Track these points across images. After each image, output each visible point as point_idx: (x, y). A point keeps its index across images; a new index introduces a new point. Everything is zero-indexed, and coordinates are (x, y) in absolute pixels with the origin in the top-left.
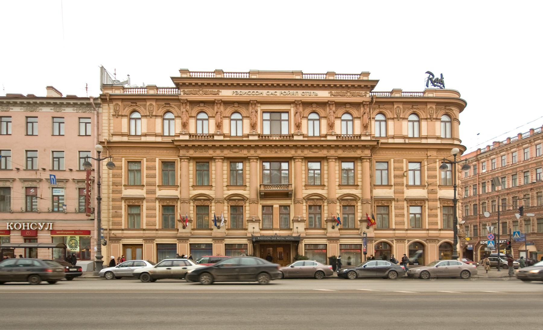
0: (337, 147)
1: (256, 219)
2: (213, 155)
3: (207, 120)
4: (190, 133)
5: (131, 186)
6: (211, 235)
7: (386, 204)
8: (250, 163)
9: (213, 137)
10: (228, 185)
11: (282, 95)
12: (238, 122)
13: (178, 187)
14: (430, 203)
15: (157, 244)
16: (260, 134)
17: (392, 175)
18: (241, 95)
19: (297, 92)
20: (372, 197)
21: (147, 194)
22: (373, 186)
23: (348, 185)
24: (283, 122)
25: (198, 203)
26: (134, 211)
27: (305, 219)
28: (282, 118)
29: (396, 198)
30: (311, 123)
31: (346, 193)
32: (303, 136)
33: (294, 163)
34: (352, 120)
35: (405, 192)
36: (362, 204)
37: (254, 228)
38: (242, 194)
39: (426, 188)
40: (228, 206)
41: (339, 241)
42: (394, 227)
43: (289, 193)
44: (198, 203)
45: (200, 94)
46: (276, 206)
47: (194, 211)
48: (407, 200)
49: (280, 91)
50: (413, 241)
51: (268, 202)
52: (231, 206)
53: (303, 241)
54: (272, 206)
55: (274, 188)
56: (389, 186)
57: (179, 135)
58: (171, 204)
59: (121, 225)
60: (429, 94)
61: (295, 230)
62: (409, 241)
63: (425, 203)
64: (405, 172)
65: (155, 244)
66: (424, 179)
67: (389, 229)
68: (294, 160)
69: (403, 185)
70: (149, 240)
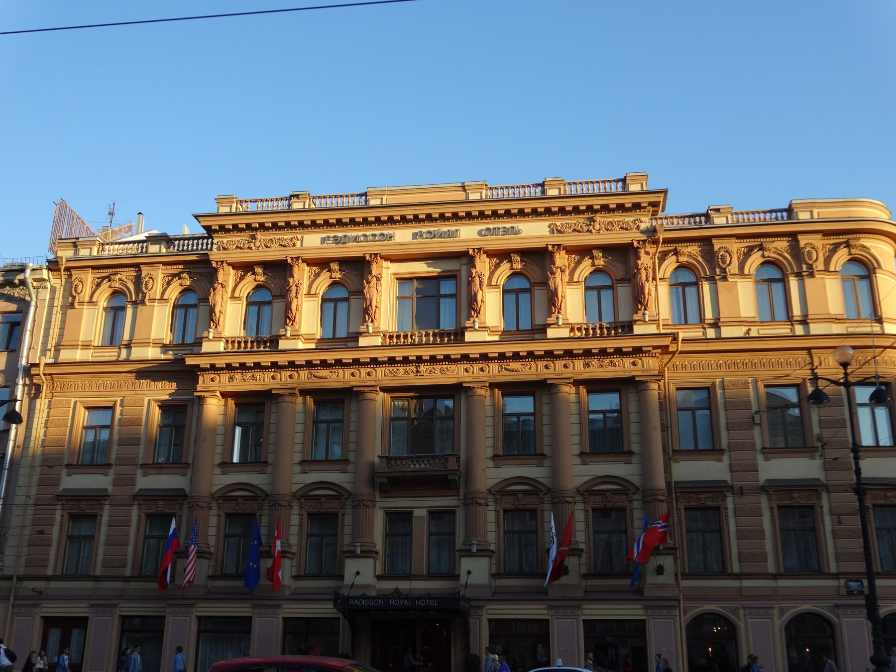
1: (363, 548)
3: (528, 290)
7: (709, 503)
8: (551, 395)
10: (144, 464)
12: (604, 293)
13: (187, 468)
14: (836, 496)
15: (200, 618)
16: (387, 331)
17: (723, 421)
20: (668, 484)
21: (114, 486)
22: (673, 454)
23: (327, 461)
24: (442, 301)
25: (508, 502)
26: (84, 529)
27: (493, 547)
28: (442, 292)
29: (737, 484)
31: (600, 474)
33: (467, 397)
34: (696, 284)
35: (760, 468)
36: (643, 503)
37: (358, 573)
38: (533, 477)
39: (817, 454)
40: (302, 515)
41: (580, 612)
42: (736, 569)
43: (450, 477)
44: (508, 502)
46: (420, 513)
47: (632, 518)
48: (767, 491)
50: (797, 609)
51: (400, 503)
52: (309, 514)
53: (484, 612)
54: (411, 513)
55: (417, 466)
56: (715, 451)
59: (46, 566)
61: (349, 578)
62: (782, 611)
63: (819, 498)
64: (756, 412)
65: (281, 619)
66: (811, 428)
67: (724, 573)
68: (466, 392)
69: (753, 448)
70: (103, 604)
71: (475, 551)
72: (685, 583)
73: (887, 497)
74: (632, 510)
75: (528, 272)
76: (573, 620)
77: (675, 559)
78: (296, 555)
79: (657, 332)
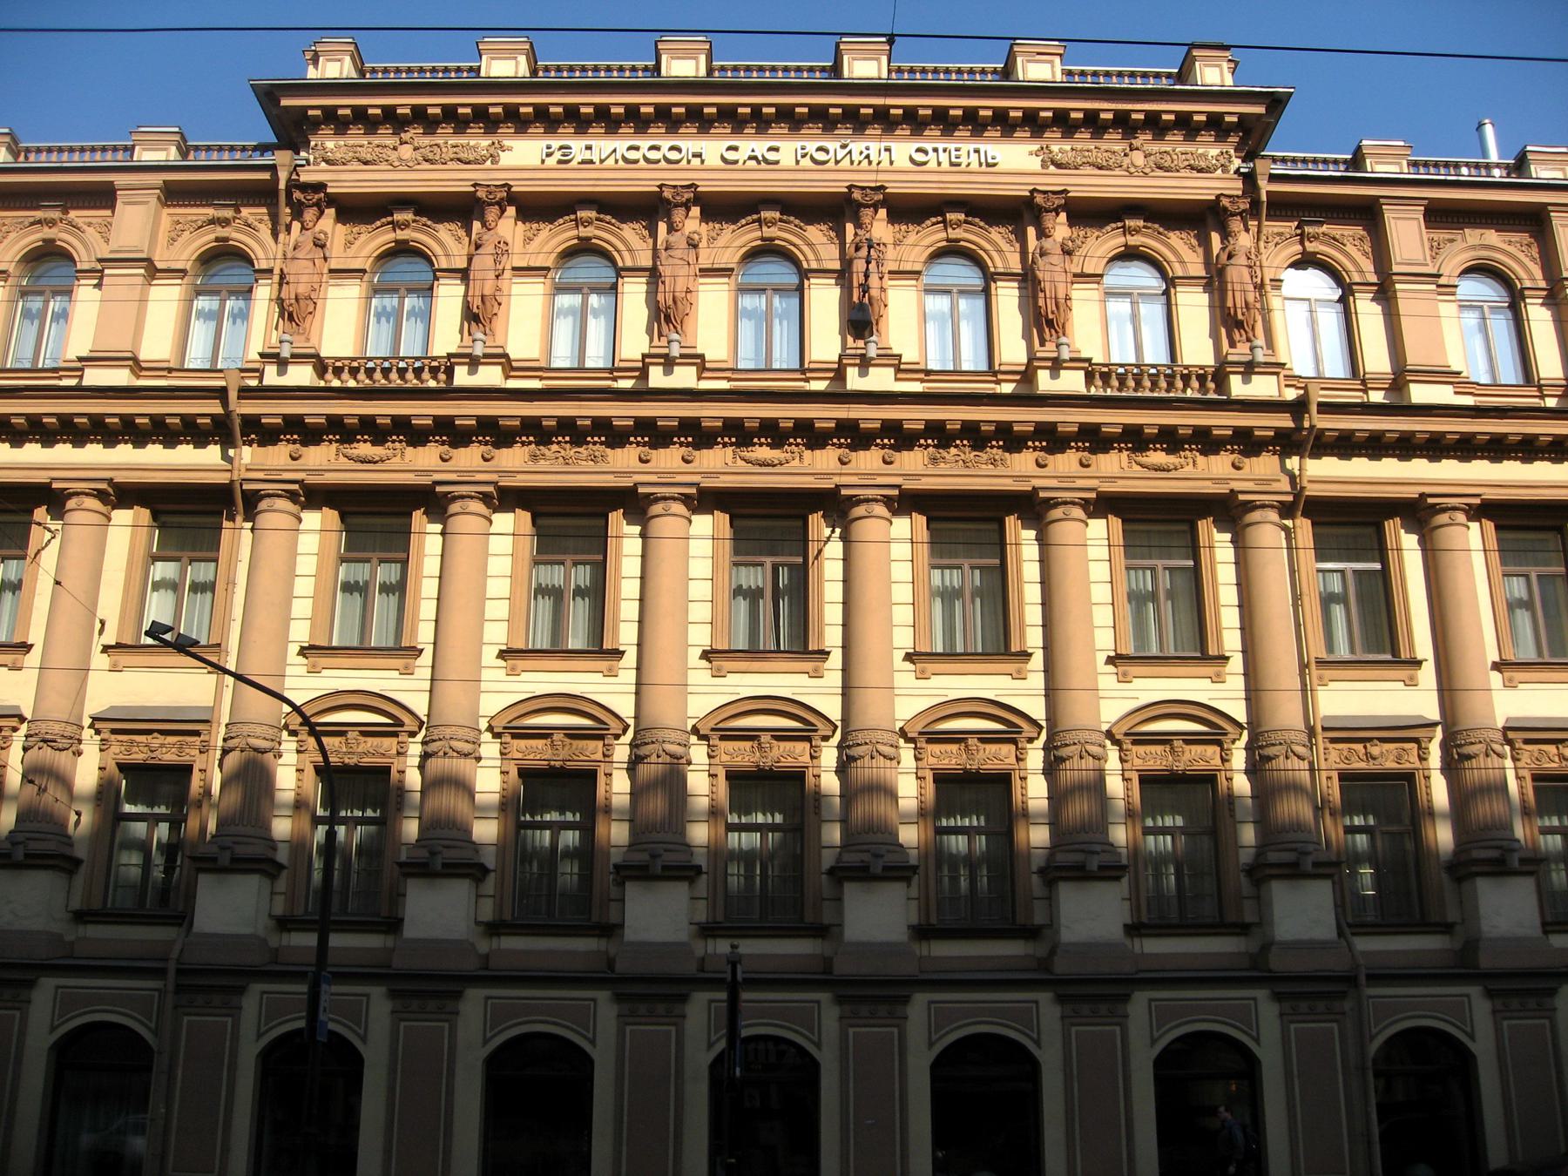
0: (939, 434)
2: (437, 477)
4: (324, 353)
5: (968, 656)
6: (831, 973)
9: (450, 372)
10: (312, 647)
11: (806, 163)
18: (591, 162)
19: (888, 150)
30: (1120, 307)
32: (898, 370)
45: (400, 159)
49: (799, 144)
57: (79, 365)
58: (169, 757)
60: (144, 153)
71: (1095, 868)
72: (1364, 944)
73: (1370, 757)
74: (1024, 779)
75: (1347, 255)
76: (1542, 1021)
77: (1334, 883)
78: (284, 873)
79: (1082, 390)
